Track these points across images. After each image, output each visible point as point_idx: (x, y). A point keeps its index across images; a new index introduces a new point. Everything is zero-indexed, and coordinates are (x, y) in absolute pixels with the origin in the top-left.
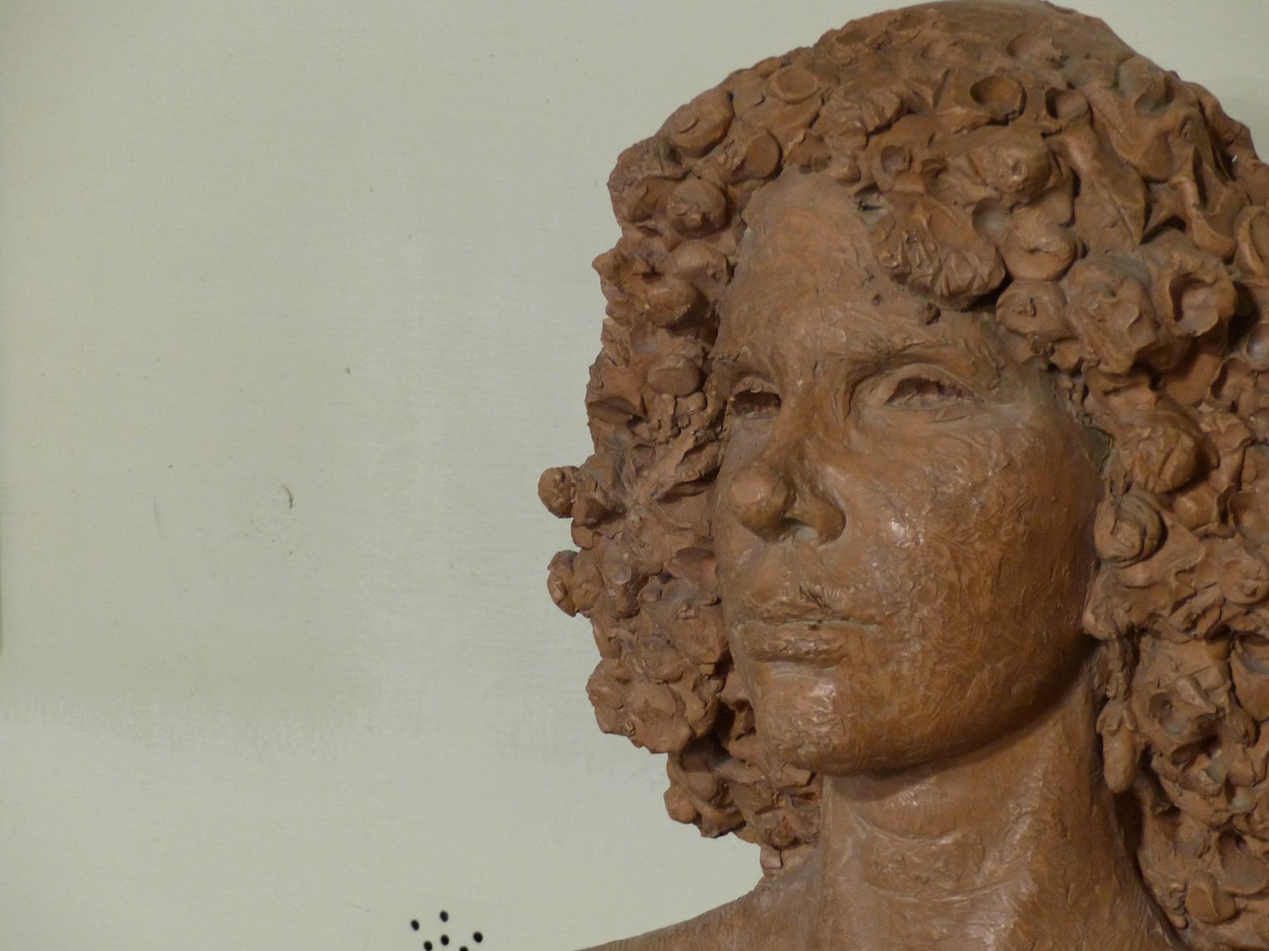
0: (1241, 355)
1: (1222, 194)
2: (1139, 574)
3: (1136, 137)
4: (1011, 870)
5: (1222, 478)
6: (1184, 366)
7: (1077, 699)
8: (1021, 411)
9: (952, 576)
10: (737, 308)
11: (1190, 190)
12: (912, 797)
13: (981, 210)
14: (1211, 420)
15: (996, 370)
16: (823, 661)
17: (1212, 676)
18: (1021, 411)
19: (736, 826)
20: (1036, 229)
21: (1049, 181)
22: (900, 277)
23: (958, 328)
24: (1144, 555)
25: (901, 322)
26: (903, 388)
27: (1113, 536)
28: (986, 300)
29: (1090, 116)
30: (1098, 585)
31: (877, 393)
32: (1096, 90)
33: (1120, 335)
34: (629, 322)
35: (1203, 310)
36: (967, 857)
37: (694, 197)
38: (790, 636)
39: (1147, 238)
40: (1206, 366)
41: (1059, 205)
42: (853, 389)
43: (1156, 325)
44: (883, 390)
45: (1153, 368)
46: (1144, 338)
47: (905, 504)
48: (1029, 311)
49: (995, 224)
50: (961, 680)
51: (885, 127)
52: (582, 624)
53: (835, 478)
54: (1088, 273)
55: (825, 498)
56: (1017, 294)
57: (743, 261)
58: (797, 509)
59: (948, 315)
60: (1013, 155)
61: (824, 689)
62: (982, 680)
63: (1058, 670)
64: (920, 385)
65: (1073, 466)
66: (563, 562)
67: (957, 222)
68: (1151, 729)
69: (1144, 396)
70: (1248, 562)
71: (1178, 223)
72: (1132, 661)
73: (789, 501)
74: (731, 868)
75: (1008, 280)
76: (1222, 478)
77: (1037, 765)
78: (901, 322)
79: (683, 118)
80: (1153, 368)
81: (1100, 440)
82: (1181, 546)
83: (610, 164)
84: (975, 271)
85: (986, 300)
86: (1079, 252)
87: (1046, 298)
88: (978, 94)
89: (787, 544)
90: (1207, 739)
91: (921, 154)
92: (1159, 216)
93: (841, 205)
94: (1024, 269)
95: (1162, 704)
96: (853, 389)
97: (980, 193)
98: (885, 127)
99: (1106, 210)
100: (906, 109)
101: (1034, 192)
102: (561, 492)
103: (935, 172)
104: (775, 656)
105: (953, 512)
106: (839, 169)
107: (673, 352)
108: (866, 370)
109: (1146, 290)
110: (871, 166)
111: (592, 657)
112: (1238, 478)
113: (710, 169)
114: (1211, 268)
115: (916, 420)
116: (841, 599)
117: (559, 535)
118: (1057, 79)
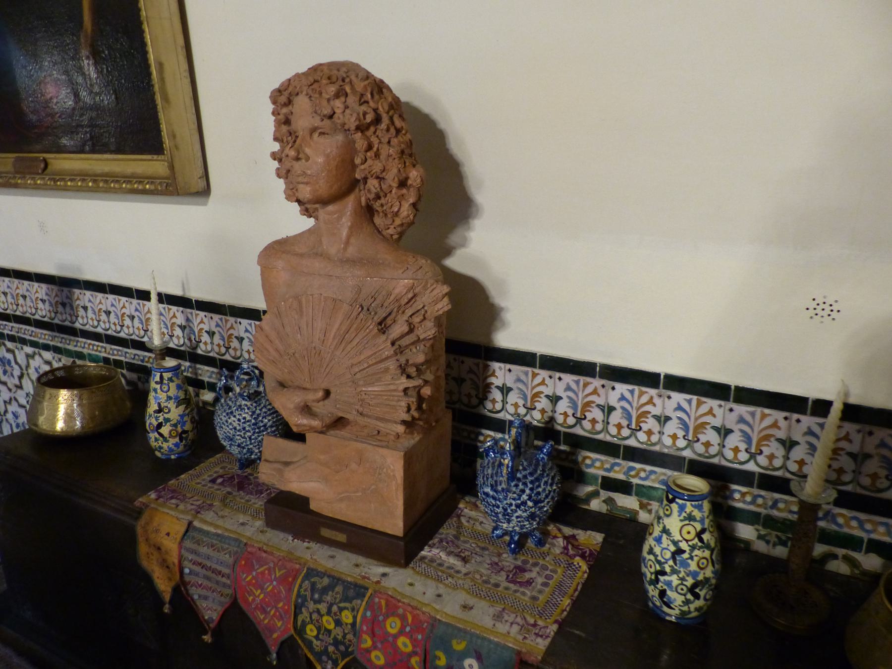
0: (378, 127)
1: (376, 97)
2: (363, 167)
3: (360, 86)
4: (346, 222)
5: (375, 149)
6: (368, 128)
7: (357, 190)
8: (340, 137)
9: (55, 101)
10: (293, 119)
11: (369, 96)
12: (330, 208)
13: (329, 100)
14: (374, 139)
15: (335, 130)
16: (307, 183)
17: (377, 185)
18: (340, 137)
19: (311, 217)
20: (338, 104)
21: (340, 93)
22: (316, 112)
23: (327, 122)
24: (362, 164)
25: (317, 122)
26: (321, 134)
27: (358, 161)
28: (331, 117)
29: (351, 82)
30: (358, 170)
31: (316, 135)
32: (353, 77)
33: (352, 123)
34: (278, 124)
35: (369, 118)
36: (339, 218)
37: (283, 99)
38: (300, 179)
39: (360, 105)
40: (372, 129)
41: (343, 99)
42: (311, 134)
43: (360, 120)
44: (317, 134)
45: (361, 128)
46: (357, 123)
47: (321, 154)
48: (339, 118)
49: (332, 102)
50: (331, 187)
51: (312, 85)
52: (282, 180)
53: (308, 150)
54: (348, 111)
55: (306, 154)
56: (336, 116)
57: (293, 111)
58: (300, 156)
59: (325, 120)
60: (332, 89)
61: (308, 189)
62: (335, 187)
63: (353, 185)
64: (324, 133)
65: (349, 149)
66: (278, 169)
67: (325, 103)
68: (369, 196)
69: (359, 134)
70: (379, 164)
71: (367, 102)
72: (365, 183)
73: (299, 154)
74: (310, 222)
75: (334, 113)
76: (375, 149)
77: (350, 203)
78: (317, 122)
79: (282, 84)
80: (361, 128)
81: (354, 142)
82: (369, 162)
83: (269, 94)
84: (327, 111)
85: (331, 117)
86: (347, 107)
87: (341, 116)
88: (329, 78)
89: (300, 162)
90: (378, 197)
91: (318, 90)
92: (362, 100)
93: (306, 100)
94: (337, 111)
95: (369, 191)
96: (311, 134)
97: (328, 97)
98: (312, 85)
99: (352, 100)
100: (316, 81)
101: (337, 96)
102: (274, 156)
103: (321, 93)
104: (298, 183)
105: (328, 156)
106: (304, 93)
107: (284, 128)
108: (313, 130)
109: (358, 114)
110: (310, 92)
111: (284, 186)
112: (378, 149)
113: (286, 94)
114: (370, 110)
115: (322, 140)
116: (309, 172)
117: (276, 164)
118: (345, 76)
